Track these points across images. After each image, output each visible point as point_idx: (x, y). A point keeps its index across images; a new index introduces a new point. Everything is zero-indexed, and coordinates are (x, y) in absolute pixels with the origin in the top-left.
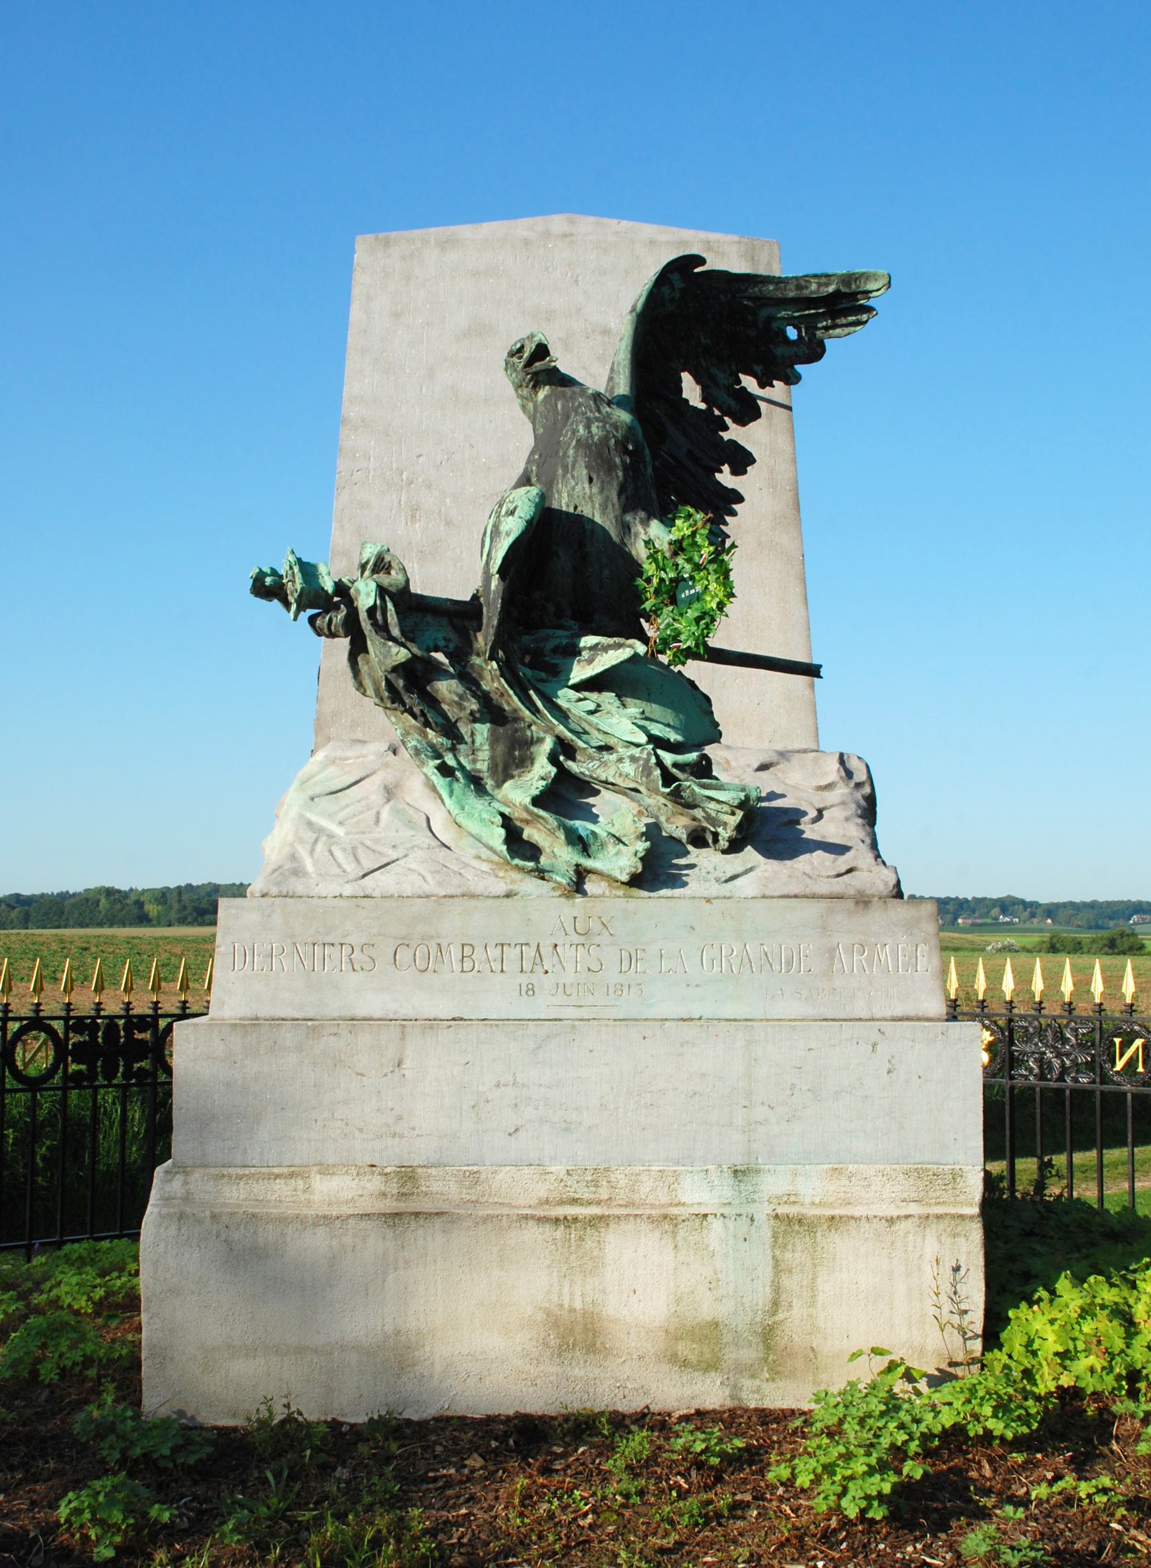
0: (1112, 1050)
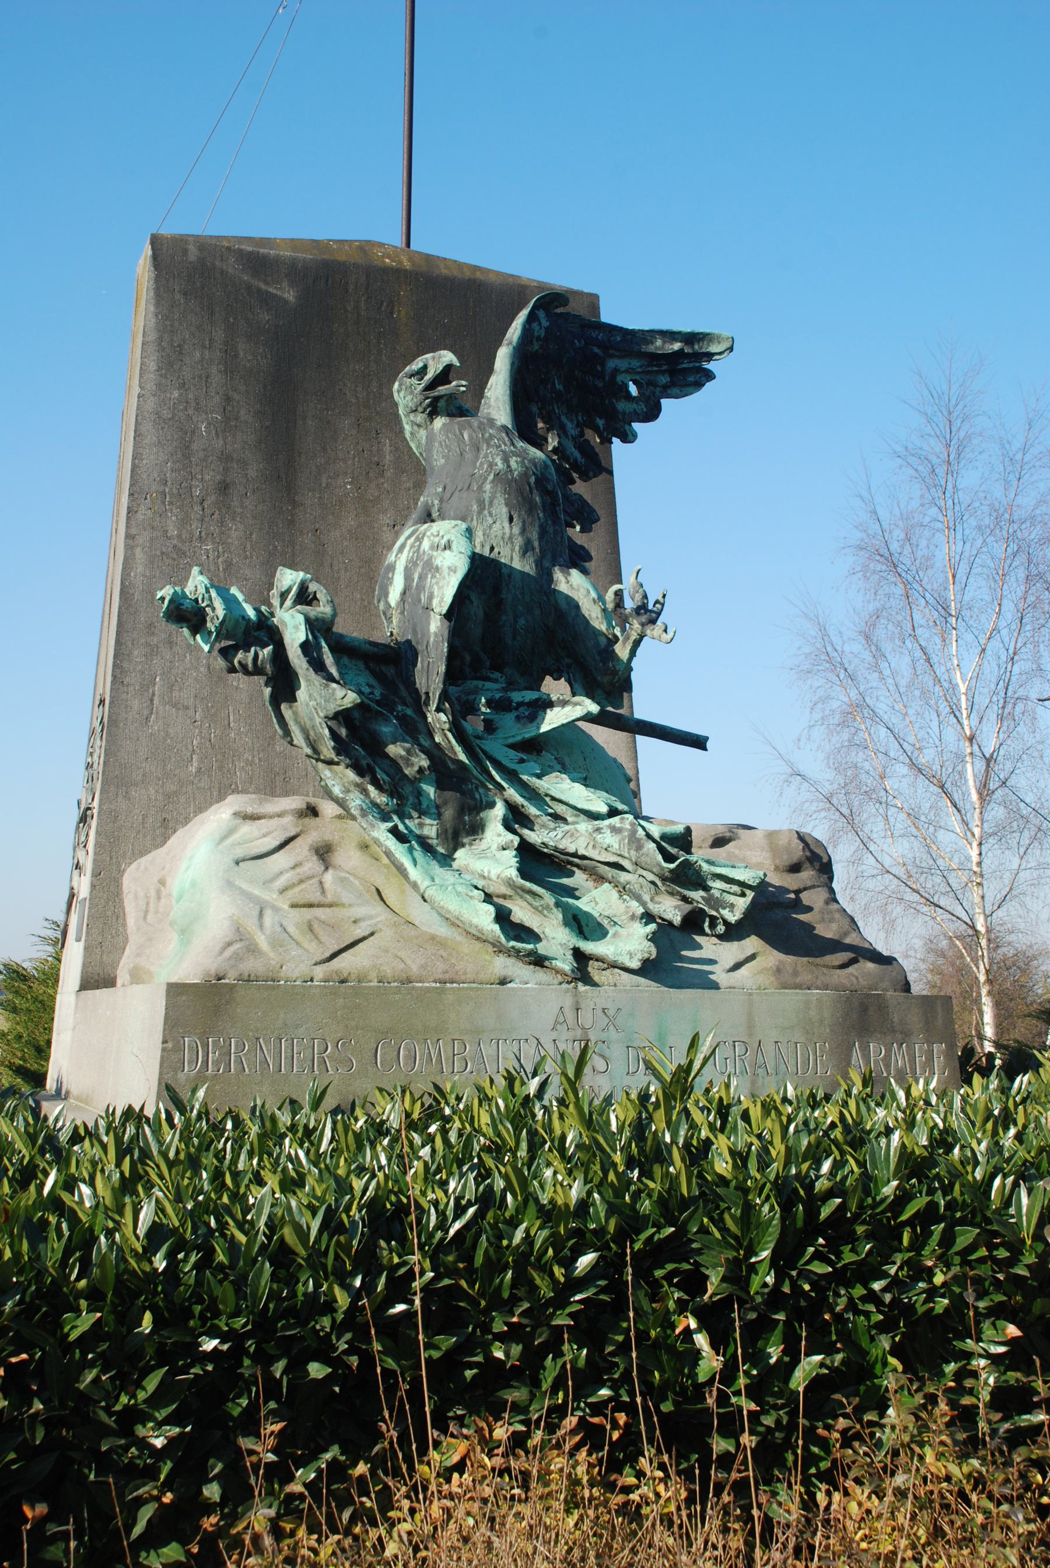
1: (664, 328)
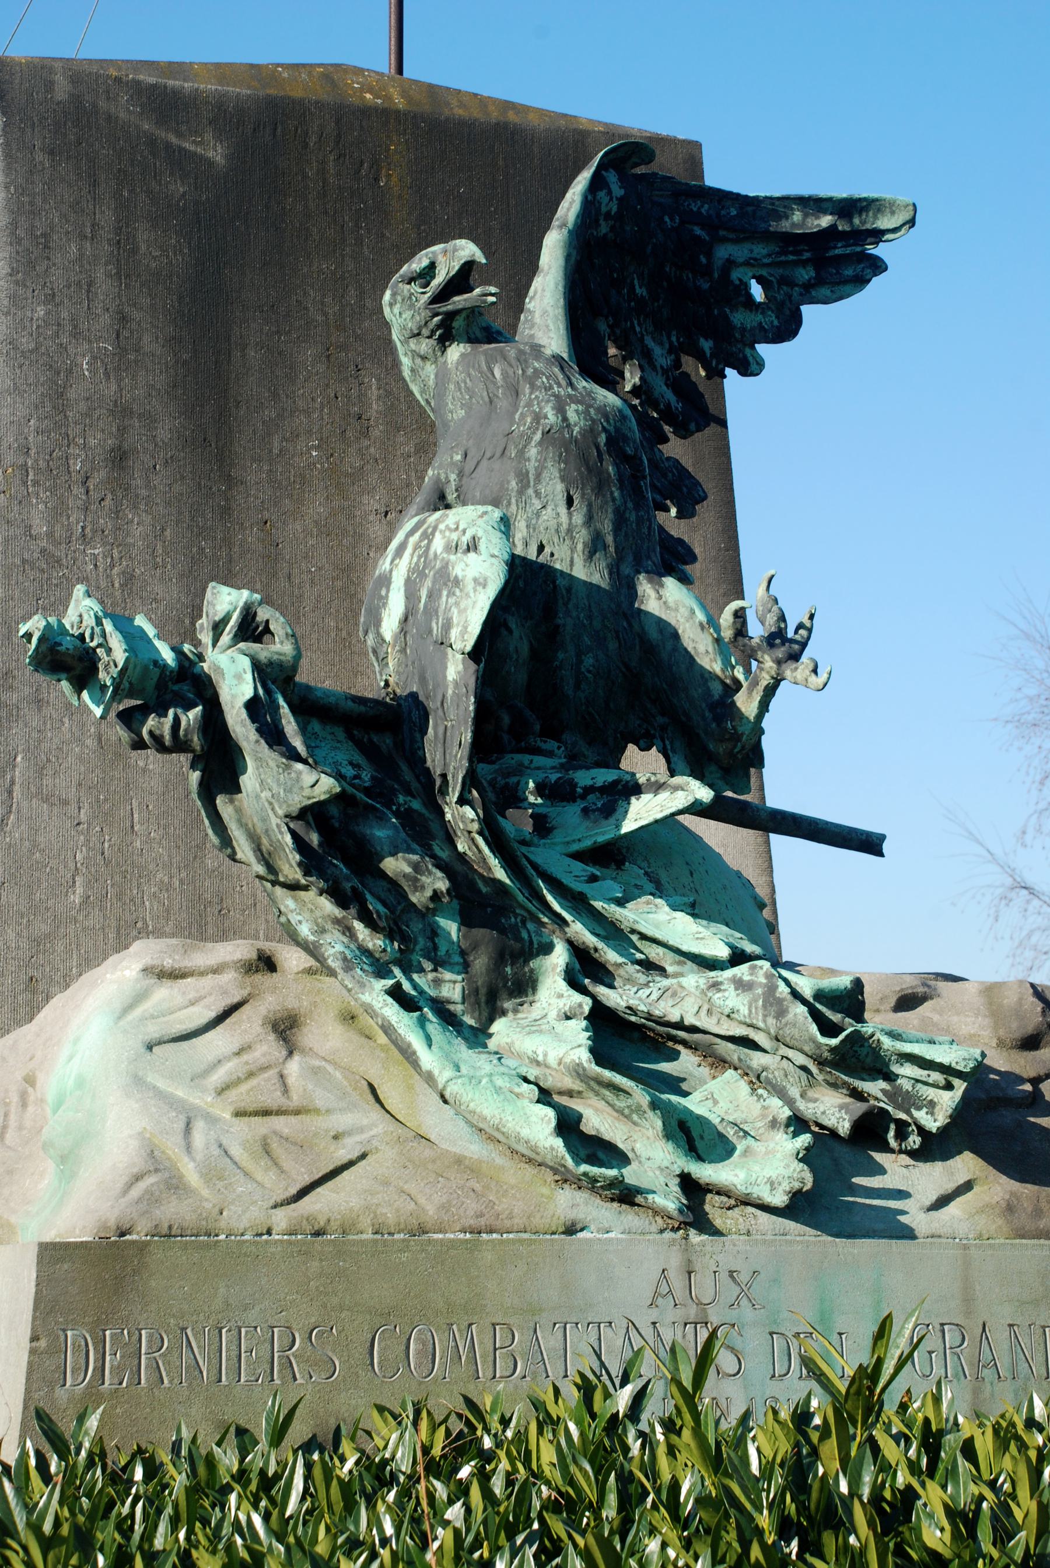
0: (383, 1344)
1: (805, 191)
